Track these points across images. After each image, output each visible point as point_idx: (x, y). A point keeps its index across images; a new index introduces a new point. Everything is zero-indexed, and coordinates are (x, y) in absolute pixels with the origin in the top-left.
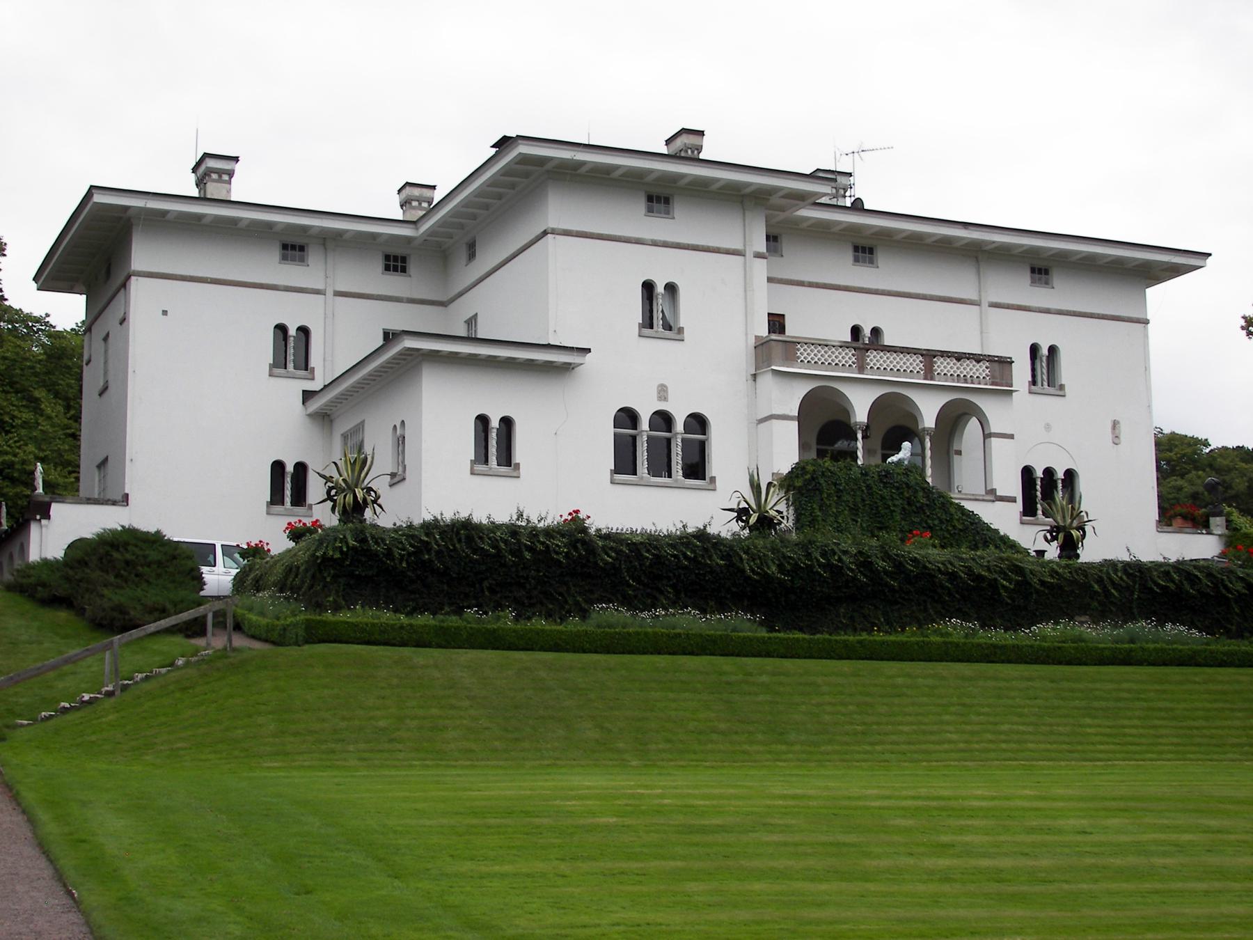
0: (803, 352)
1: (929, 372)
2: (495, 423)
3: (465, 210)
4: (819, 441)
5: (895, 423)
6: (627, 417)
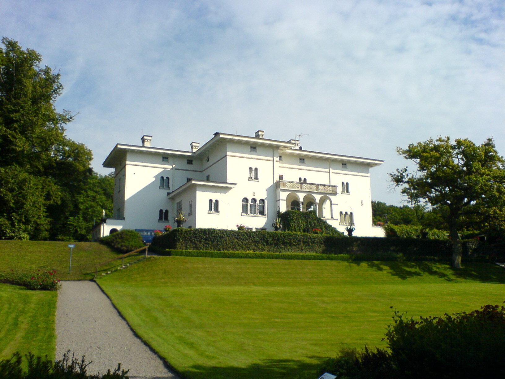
0: (287, 184)
1: (317, 189)
2: (214, 201)
3: (194, 370)
4: (291, 205)
5: (310, 202)
6: (246, 200)
